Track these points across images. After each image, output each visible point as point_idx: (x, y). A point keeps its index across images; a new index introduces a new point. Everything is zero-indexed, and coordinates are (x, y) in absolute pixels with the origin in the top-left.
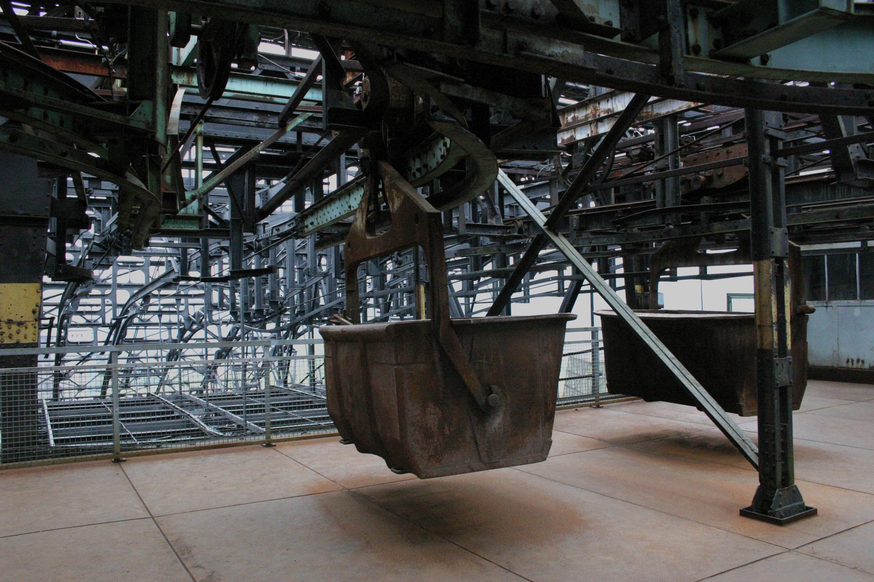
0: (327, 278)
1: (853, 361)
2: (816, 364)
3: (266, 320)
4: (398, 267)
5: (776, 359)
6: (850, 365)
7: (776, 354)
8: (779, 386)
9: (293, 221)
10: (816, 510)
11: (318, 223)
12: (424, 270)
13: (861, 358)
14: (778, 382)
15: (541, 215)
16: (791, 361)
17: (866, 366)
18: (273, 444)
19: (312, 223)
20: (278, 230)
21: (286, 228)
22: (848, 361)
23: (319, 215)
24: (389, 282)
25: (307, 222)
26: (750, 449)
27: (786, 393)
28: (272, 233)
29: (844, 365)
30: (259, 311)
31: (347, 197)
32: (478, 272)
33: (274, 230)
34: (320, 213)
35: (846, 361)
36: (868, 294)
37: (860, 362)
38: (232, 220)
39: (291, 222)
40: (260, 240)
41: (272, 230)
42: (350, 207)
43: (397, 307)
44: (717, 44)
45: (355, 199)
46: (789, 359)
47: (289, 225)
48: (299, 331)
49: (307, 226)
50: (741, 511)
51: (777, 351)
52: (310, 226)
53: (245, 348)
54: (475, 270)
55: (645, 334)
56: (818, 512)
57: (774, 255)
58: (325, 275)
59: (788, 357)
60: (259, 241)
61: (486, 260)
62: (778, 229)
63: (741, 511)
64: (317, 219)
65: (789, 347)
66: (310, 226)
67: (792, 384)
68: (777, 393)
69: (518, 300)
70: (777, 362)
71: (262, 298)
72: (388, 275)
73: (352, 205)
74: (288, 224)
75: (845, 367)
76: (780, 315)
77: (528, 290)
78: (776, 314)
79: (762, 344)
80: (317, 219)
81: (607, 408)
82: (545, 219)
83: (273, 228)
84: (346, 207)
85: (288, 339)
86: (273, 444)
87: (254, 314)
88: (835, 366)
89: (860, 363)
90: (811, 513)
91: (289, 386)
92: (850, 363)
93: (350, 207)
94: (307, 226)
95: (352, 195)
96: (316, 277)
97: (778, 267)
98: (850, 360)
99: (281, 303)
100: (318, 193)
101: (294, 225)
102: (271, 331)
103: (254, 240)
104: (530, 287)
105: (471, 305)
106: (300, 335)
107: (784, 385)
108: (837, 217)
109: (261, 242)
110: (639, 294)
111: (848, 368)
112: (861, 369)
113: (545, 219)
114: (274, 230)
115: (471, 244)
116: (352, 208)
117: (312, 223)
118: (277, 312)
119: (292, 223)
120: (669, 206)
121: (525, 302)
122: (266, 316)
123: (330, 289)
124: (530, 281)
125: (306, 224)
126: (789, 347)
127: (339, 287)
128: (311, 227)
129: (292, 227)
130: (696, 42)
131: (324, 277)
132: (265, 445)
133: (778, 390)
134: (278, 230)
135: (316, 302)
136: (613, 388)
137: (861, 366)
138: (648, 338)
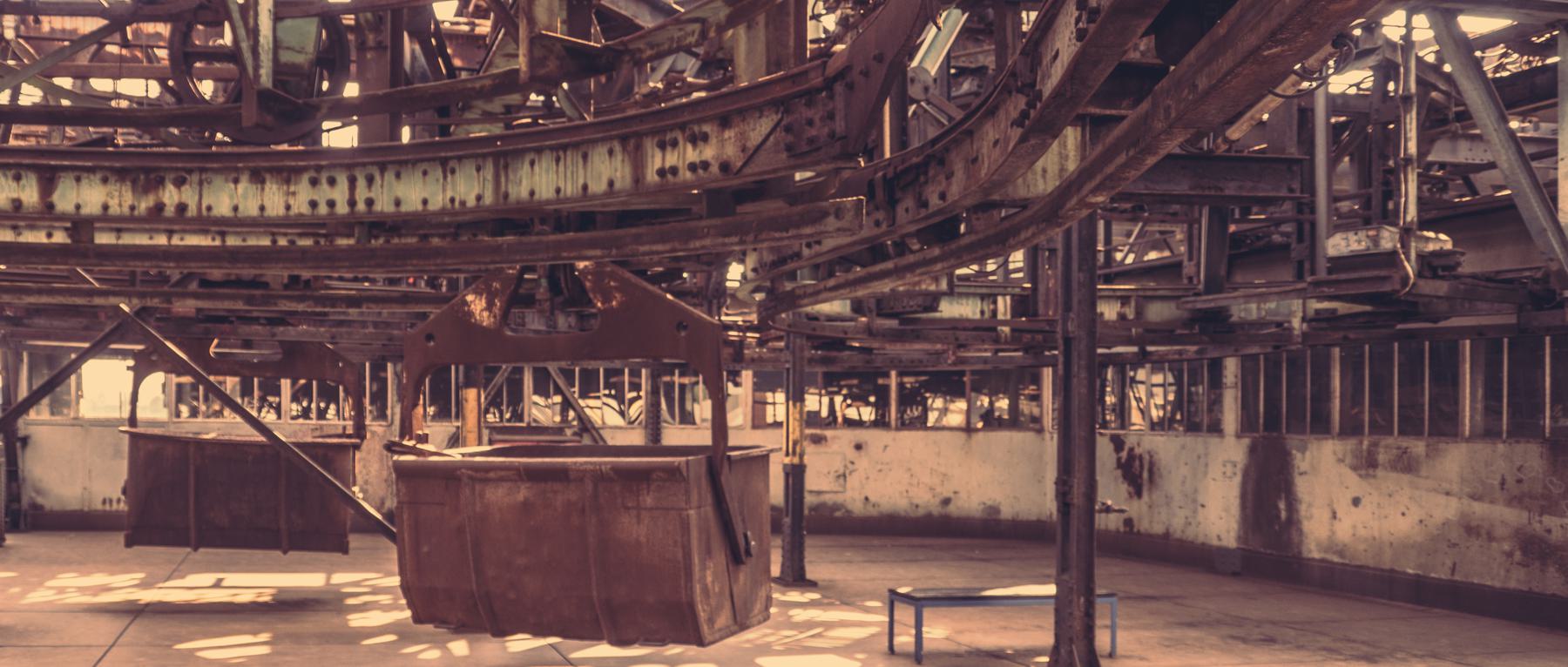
1: (111, 501)
6: (107, 507)
22: (104, 502)
29: (99, 506)
88: (86, 509)
111: (105, 511)
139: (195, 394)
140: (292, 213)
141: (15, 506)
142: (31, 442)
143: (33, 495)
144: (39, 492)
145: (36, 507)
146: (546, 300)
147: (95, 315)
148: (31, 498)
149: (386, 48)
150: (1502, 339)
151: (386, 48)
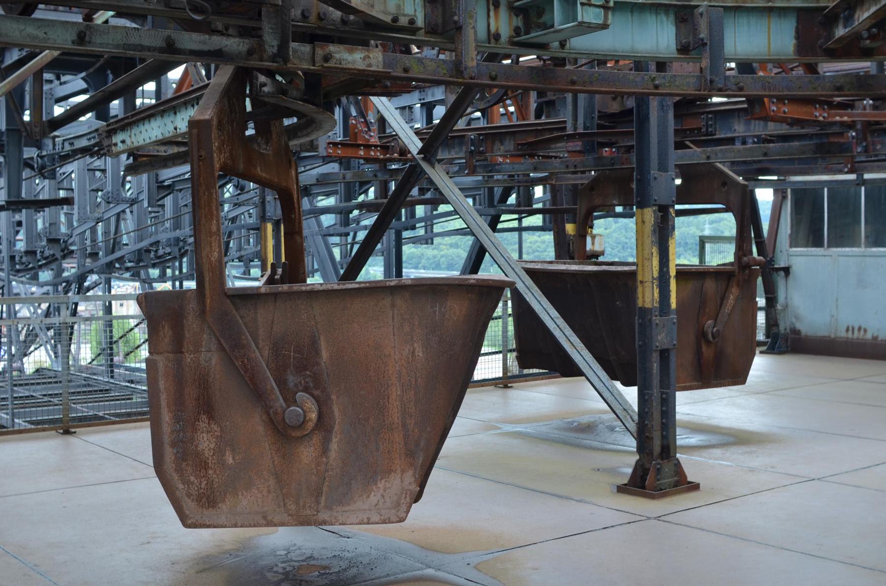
0: (135, 206)
1: (853, 329)
2: (809, 334)
3: (40, 267)
4: (239, 194)
5: (656, 320)
6: (850, 335)
7: (657, 313)
8: (659, 349)
9: (95, 134)
10: (699, 485)
11: (133, 143)
12: (273, 203)
13: (863, 326)
14: (658, 344)
15: (416, 139)
16: (675, 320)
17: (869, 336)
18: (73, 430)
19: (123, 142)
20: (72, 144)
21: (83, 143)
22: (847, 330)
23: (133, 132)
24: (227, 212)
25: (117, 138)
26: (630, 420)
27: (668, 357)
28: (63, 148)
29: (843, 334)
30: (30, 253)
31: (172, 115)
32: (349, 204)
33: (66, 144)
34: (135, 130)
35: (845, 328)
36: (875, 241)
37: (862, 330)
38: (7, 130)
39: (93, 135)
40: (44, 156)
41: (63, 144)
42: (176, 129)
43: (240, 249)
44: (517, 31)
45: (183, 119)
46: (673, 318)
47: (89, 139)
48: (86, 284)
49: (116, 145)
50: (618, 487)
51: (658, 310)
52: (120, 144)
53: (12, 306)
54: (346, 201)
55: (527, 290)
56: (701, 486)
57: (657, 203)
58: (133, 202)
59: (672, 316)
60: (42, 157)
61: (363, 186)
62: (664, 174)
63: (618, 487)
64: (130, 136)
65: (674, 305)
66: (120, 144)
67: (676, 346)
68: (655, 357)
69: (415, 241)
70: (657, 321)
71: (34, 234)
72: (225, 205)
73: (179, 126)
74: (89, 137)
75: (843, 338)
76: (665, 269)
77: (432, 225)
78: (657, 268)
79: (644, 301)
80: (130, 136)
81: (517, 389)
82: (420, 144)
83: (64, 140)
84: (171, 128)
85: (70, 294)
86: (73, 430)
87: (21, 257)
88: (833, 336)
89: (862, 332)
90: (695, 487)
91: (72, 368)
92: (850, 332)
93: (176, 129)
94: (116, 145)
95: (178, 114)
96: (118, 204)
97: (661, 216)
98: (851, 329)
99: (64, 242)
100: (129, 104)
101: (97, 140)
102: (46, 284)
103: (35, 156)
104: (435, 221)
105: (349, 246)
106: (88, 289)
107: (665, 347)
108: (765, 154)
109: (46, 159)
110: (571, 235)
111: (847, 338)
112: (862, 339)
113: (420, 144)
114: (66, 144)
115: (341, 164)
116: (178, 130)
117: (123, 142)
118: (59, 255)
119: (94, 138)
120: (580, 130)
121: (427, 243)
122: (39, 261)
123: (139, 221)
124: (435, 213)
125: (114, 141)
126: (674, 305)
127: (152, 218)
128: (121, 147)
129: (93, 142)
130: (497, 29)
131: (132, 205)
132: (61, 431)
133: (658, 353)
134: (72, 144)
135: (118, 240)
136: (523, 363)
137: (863, 335)
138: (530, 294)
139: (523, 204)
140: (144, 318)
141: (775, 330)
142: (791, 270)
143: (794, 320)
144: (797, 318)
145: (796, 332)
146: (190, 236)
147: (156, 257)
148: (792, 323)
149: (706, 44)
150: (787, 189)
151: (706, 44)
